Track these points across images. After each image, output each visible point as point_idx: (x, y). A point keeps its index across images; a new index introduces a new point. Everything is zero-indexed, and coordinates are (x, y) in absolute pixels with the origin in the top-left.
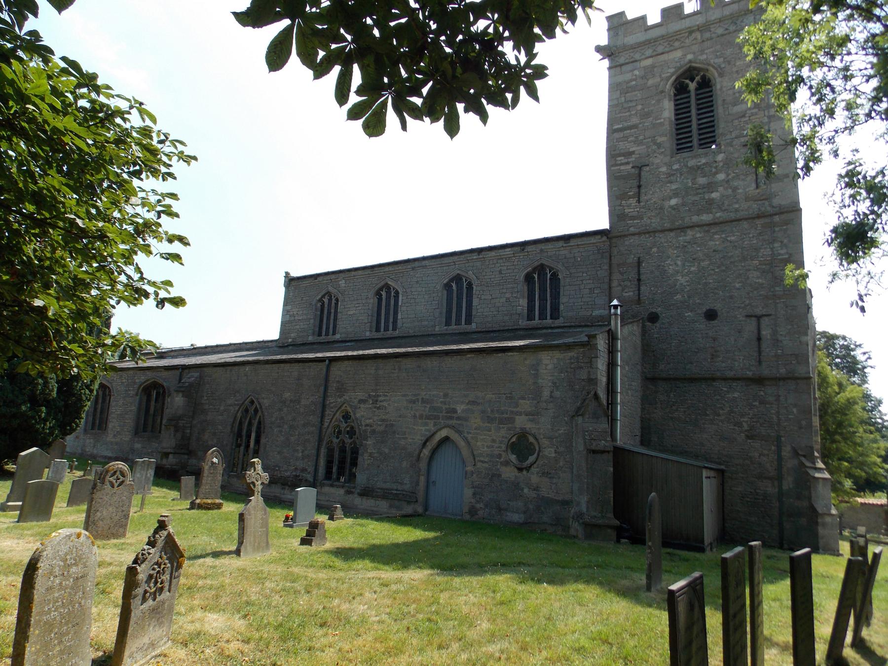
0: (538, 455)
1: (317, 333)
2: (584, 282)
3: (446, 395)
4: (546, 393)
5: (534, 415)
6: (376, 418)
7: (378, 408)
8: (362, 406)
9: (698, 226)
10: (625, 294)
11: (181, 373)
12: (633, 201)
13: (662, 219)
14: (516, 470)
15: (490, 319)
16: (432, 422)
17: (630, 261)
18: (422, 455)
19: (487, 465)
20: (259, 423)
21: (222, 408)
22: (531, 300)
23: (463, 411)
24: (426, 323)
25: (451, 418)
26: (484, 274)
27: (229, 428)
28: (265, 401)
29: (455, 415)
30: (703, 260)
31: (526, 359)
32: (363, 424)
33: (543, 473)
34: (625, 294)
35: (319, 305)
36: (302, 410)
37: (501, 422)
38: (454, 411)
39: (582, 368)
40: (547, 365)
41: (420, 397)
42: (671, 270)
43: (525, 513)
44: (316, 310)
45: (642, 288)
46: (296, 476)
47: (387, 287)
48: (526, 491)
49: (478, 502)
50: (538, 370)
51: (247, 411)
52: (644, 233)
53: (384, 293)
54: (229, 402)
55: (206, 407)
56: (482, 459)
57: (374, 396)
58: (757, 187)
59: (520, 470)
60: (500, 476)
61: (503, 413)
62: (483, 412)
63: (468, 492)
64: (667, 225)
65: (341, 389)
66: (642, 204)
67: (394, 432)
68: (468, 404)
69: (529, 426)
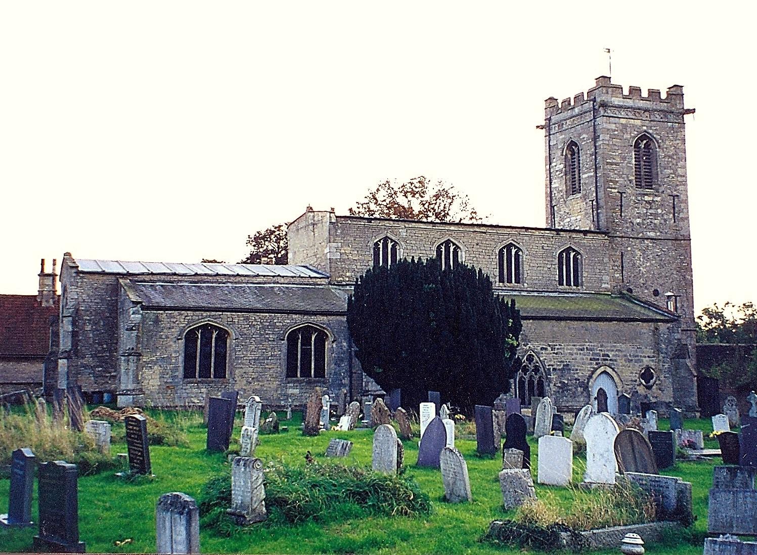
32: (547, 364)
58: (675, 222)
60: (637, 392)
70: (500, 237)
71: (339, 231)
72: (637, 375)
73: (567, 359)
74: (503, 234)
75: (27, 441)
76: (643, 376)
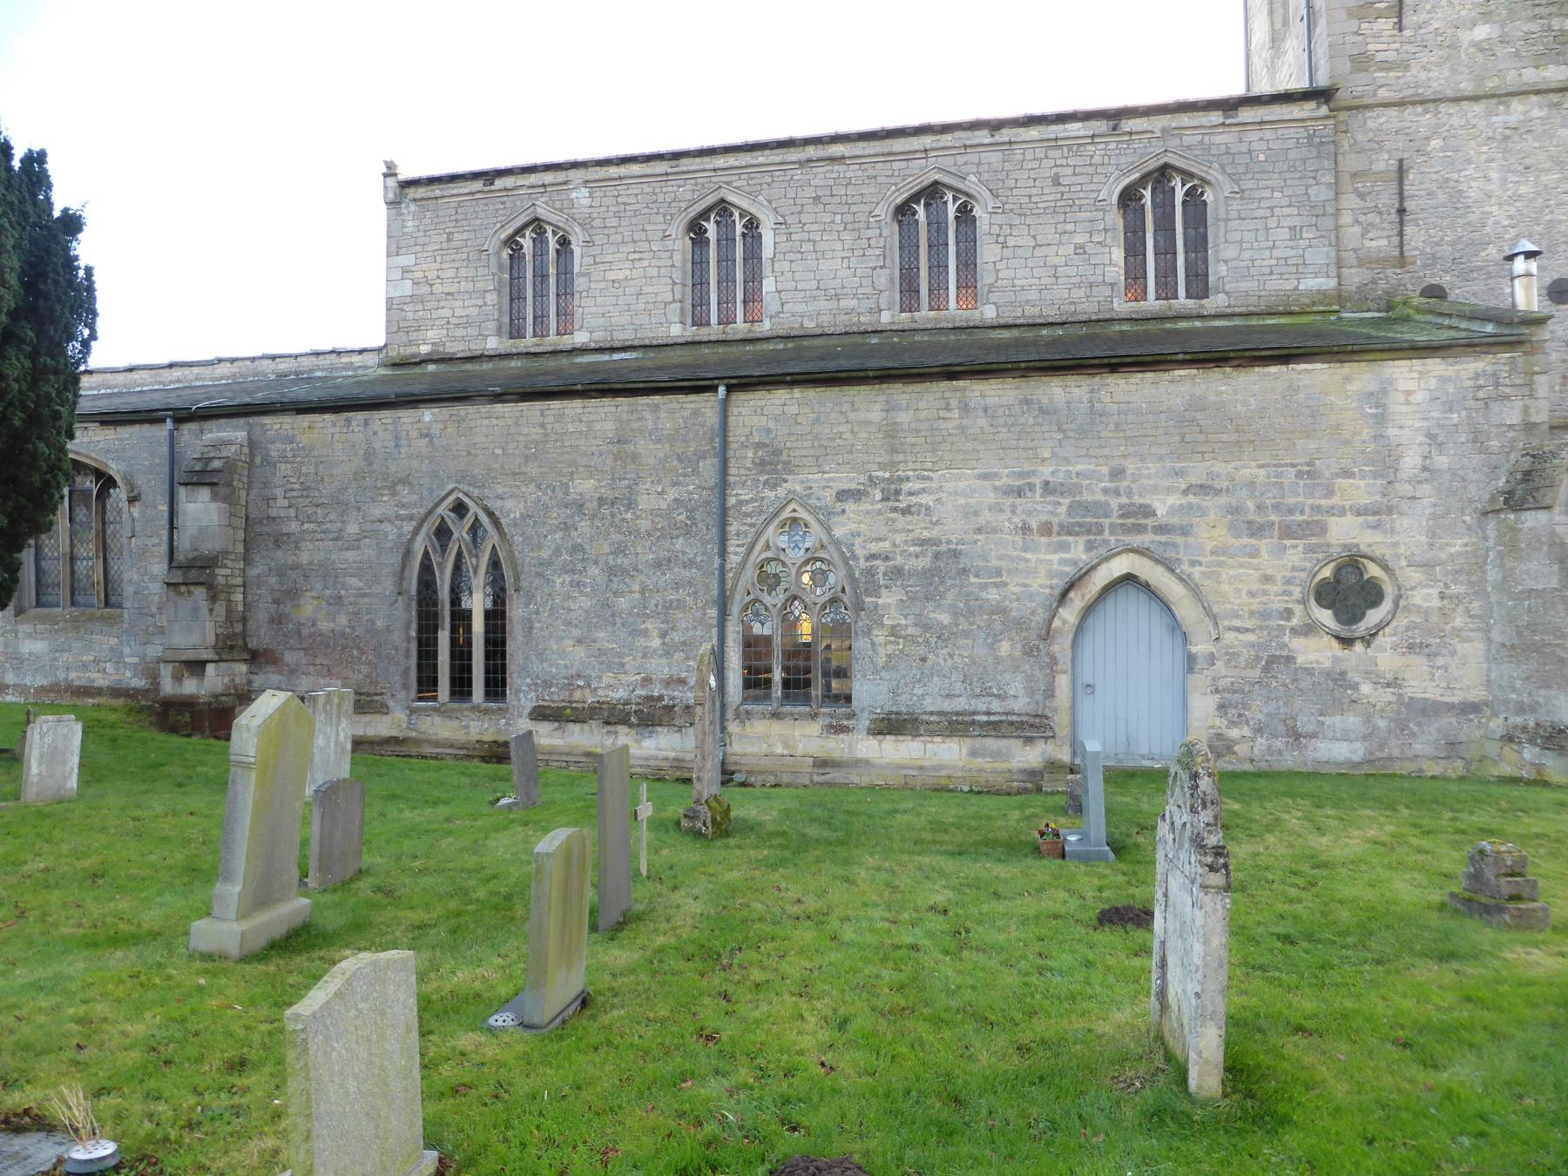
0: (1396, 604)
1: (506, 328)
2: (1277, 211)
3: (1117, 473)
4: (1411, 462)
5: (1378, 513)
6: (899, 538)
7: (906, 511)
8: (849, 506)
9: (1537, 92)
10: (1368, 244)
11: (171, 433)
12: (1386, 25)
13: (1453, 70)
14: (1335, 643)
15: (1033, 295)
16: (1081, 541)
17: (1380, 166)
18: (1056, 623)
19: (1251, 638)
20: (495, 564)
21: (352, 529)
22: (1134, 249)
23: (1173, 511)
24: (854, 303)
25: (1140, 529)
26: (1011, 183)
27: (388, 585)
28: (509, 504)
29: (1149, 522)
30: (1547, 171)
31: (1348, 379)
32: (859, 552)
33: (1411, 647)
34: (1368, 244)
35: (506, 252)
36: (644, 525)
37: (1288, 532)
38: (1148, 512)
39: (1507, 397)
40: (1409, 393)
41: (1037, 481)
42: (1473, 192)
43: (1364, 738)
44: (500, 266)
45: (1408, 230)
46: (650, 698)
47: (722, 208)
48: (1366, 688)
49: (1232, 724)
50: (1384, 406)
51: (443, 533)
52: (1413, 103)
53: (527, 242)
54: (377, 511)
55: (293, 527)
56: (1237, 623)
57: (890, 481)
59: (1346, 642)
60: (1290, 659)
61: (1291, 511)
62: (1235, 510)
63: (1203, 706)
64: (1467, 87)
65: (773, 463)
66: (1407, 33)
67: (964, 571)
68: (1186, 492)
69: (1367, 540)
70: (896, 165)
71: (410, 224)
73: (952, 529)
74: (908, 156)
76: (1327, 594)
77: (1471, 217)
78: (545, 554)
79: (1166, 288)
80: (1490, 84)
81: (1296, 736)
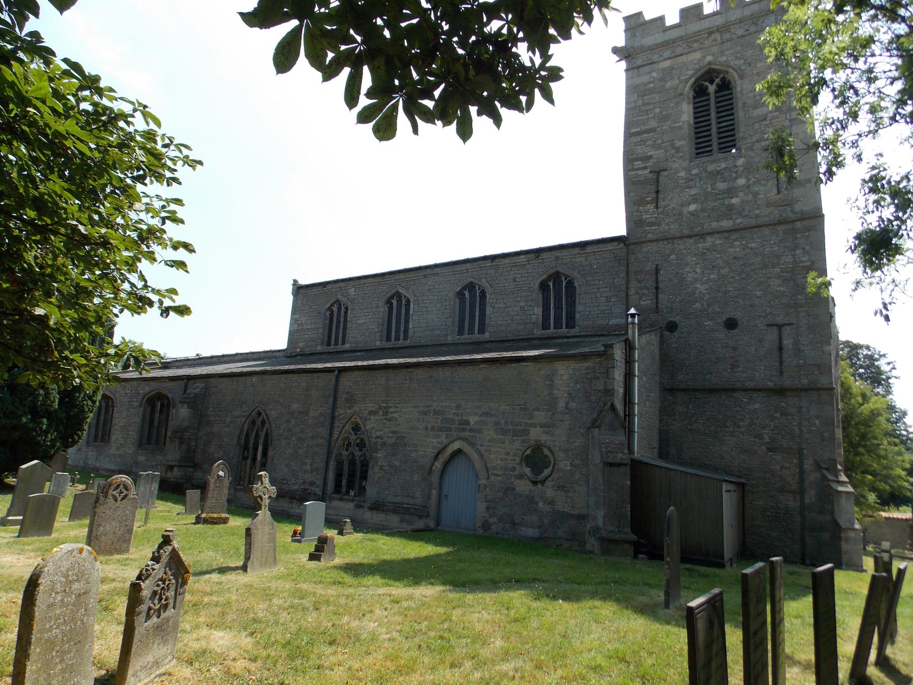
0: (553, 468)
2: (601, 290)
3: (458, 407)
4: (561, 405)
5: (549, 427)
7: (389, 420)
8: (372, 417)
9: (718, 232)
10: (642, 303)
11: (186, 384)
12: (651, 207)
13: (680, 225)
14: (530, 484)
15: (503, 328)
16: (444, 434)
17: (647, 268)
18: (434, 468)
19: (500, 479)
20: (267, 435)
21: (228, 420)
22: (546, 308)
23: (476, 423)
24: (438, 332)
25: (464, 430)
26: (497, 281)
27: (235, 440)
28: (273, 412)
29: (468, 427)
30: (723, 268)
31: (540, 369)
32: (374, 436)
33: (558, 487)
34: (642, 303)
35: (328, 313)
36: (310, 422)
37: (516, 434)
38: (467, 423)
39: (598, 378)
40: (562, 375)
41: (432, 409)
42: (690, 277)
43: (539, 527)
45: (660, 296)
46: (305, 489)
47: (398, 295)
48: (541, 505)
49: (491, 516)
50: (553, 381)
51: (254, 422)
52: (663, 240)
53: (394, 302)
54: (236, 413)
55: (212, 418)
56: (496, 472)
57: (385, 408)
58: (778, 193)
59: (535, 483)
60: (514, 489)
61: (517, 425)
62: (497, 424)
63: (481, 506)
64: (686, 232)
65: (351, 400)
66: (660, 210)
67: (405, 445)
68: (481, 415)
69: (543, 438)
72: (518, 459)
75: (381, 657)
77: (689, 290)
78: (281, 431)
79: (558, 325)
80: (697, 230)
81: (514, 524)
